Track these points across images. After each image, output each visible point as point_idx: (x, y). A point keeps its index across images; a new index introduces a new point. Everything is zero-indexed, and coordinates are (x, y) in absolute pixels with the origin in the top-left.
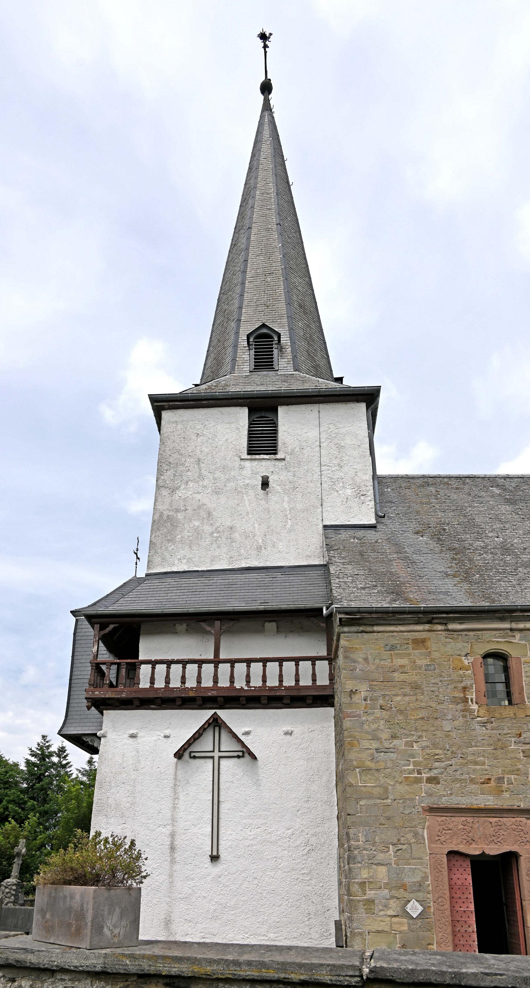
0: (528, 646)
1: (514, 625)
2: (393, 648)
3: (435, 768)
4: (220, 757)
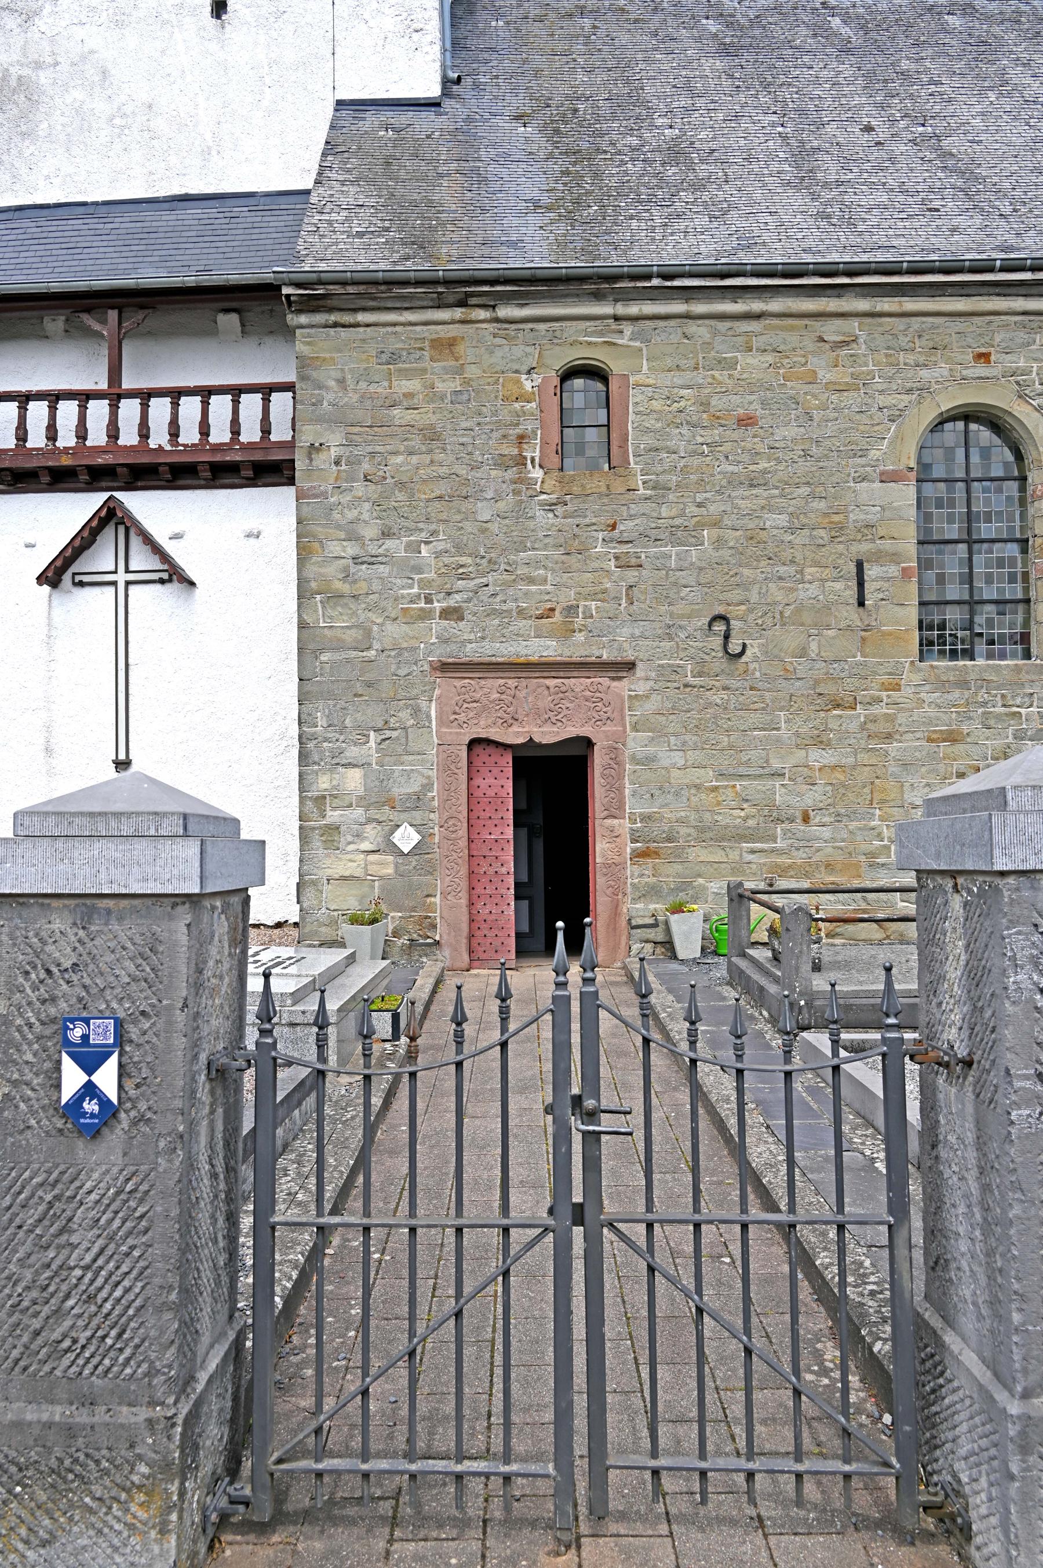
0: (645, 352)
1: (621, 309)
2: (394, 358)
3: (457, 592)
4: (128, 583)
